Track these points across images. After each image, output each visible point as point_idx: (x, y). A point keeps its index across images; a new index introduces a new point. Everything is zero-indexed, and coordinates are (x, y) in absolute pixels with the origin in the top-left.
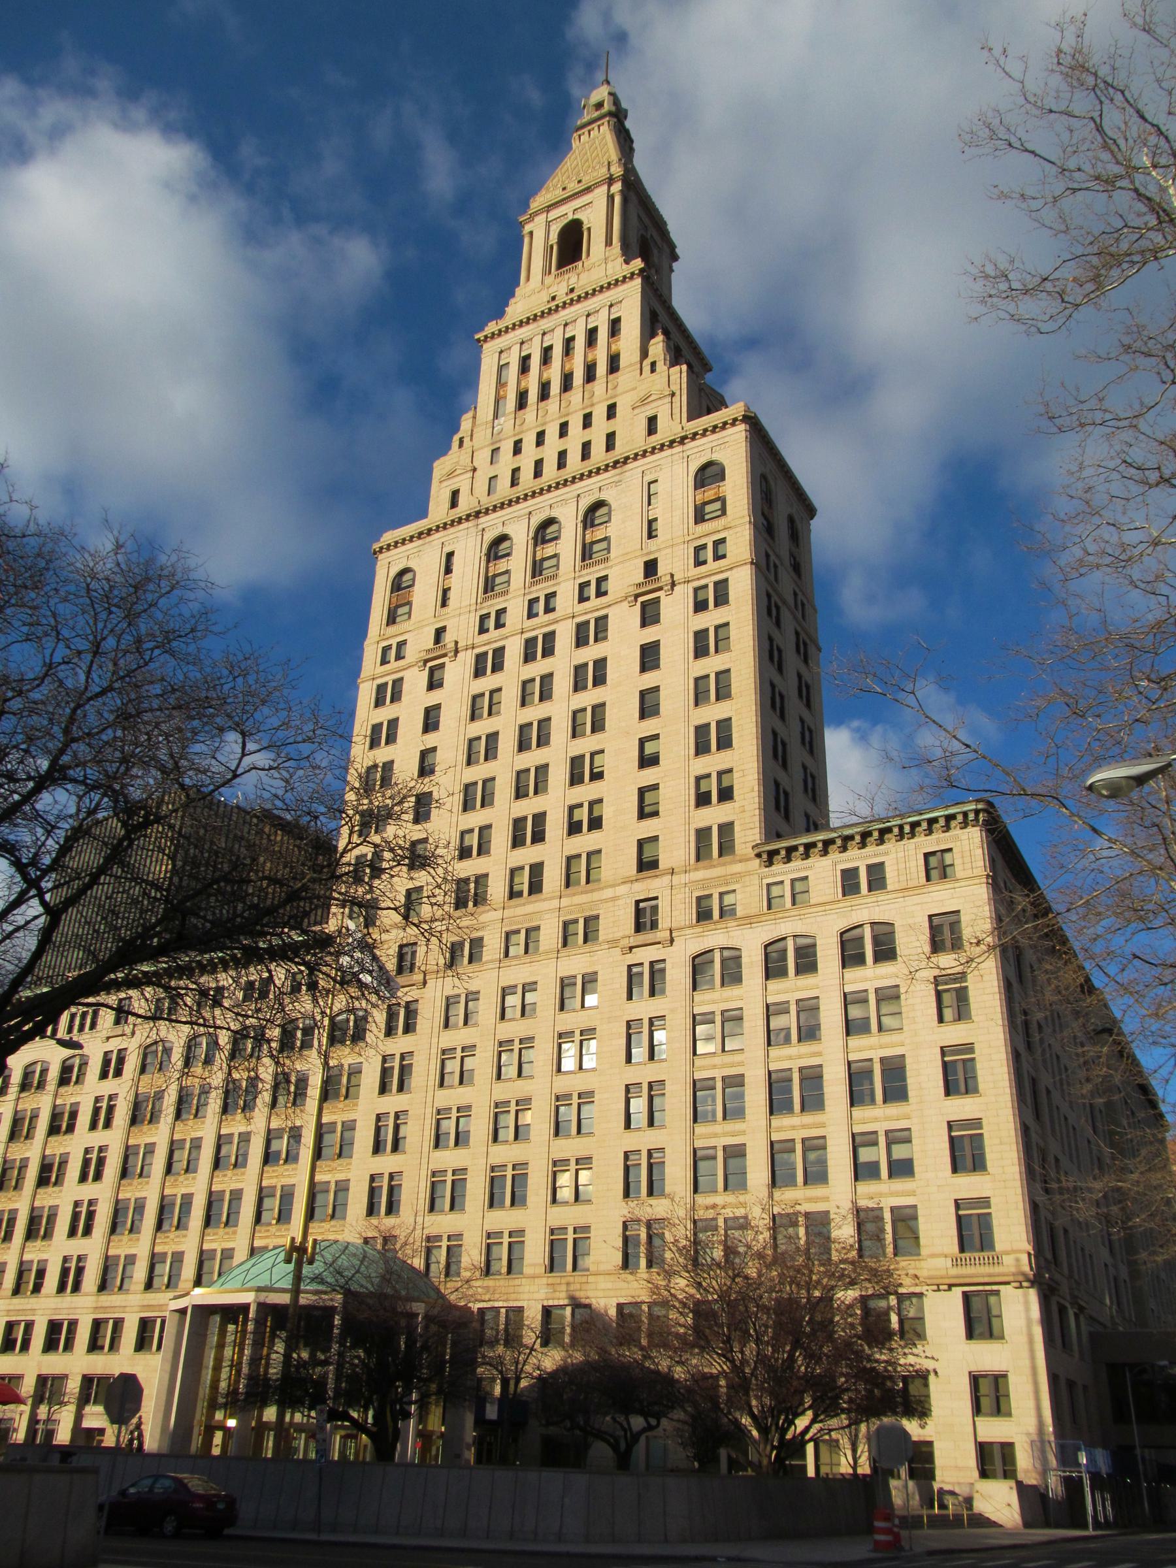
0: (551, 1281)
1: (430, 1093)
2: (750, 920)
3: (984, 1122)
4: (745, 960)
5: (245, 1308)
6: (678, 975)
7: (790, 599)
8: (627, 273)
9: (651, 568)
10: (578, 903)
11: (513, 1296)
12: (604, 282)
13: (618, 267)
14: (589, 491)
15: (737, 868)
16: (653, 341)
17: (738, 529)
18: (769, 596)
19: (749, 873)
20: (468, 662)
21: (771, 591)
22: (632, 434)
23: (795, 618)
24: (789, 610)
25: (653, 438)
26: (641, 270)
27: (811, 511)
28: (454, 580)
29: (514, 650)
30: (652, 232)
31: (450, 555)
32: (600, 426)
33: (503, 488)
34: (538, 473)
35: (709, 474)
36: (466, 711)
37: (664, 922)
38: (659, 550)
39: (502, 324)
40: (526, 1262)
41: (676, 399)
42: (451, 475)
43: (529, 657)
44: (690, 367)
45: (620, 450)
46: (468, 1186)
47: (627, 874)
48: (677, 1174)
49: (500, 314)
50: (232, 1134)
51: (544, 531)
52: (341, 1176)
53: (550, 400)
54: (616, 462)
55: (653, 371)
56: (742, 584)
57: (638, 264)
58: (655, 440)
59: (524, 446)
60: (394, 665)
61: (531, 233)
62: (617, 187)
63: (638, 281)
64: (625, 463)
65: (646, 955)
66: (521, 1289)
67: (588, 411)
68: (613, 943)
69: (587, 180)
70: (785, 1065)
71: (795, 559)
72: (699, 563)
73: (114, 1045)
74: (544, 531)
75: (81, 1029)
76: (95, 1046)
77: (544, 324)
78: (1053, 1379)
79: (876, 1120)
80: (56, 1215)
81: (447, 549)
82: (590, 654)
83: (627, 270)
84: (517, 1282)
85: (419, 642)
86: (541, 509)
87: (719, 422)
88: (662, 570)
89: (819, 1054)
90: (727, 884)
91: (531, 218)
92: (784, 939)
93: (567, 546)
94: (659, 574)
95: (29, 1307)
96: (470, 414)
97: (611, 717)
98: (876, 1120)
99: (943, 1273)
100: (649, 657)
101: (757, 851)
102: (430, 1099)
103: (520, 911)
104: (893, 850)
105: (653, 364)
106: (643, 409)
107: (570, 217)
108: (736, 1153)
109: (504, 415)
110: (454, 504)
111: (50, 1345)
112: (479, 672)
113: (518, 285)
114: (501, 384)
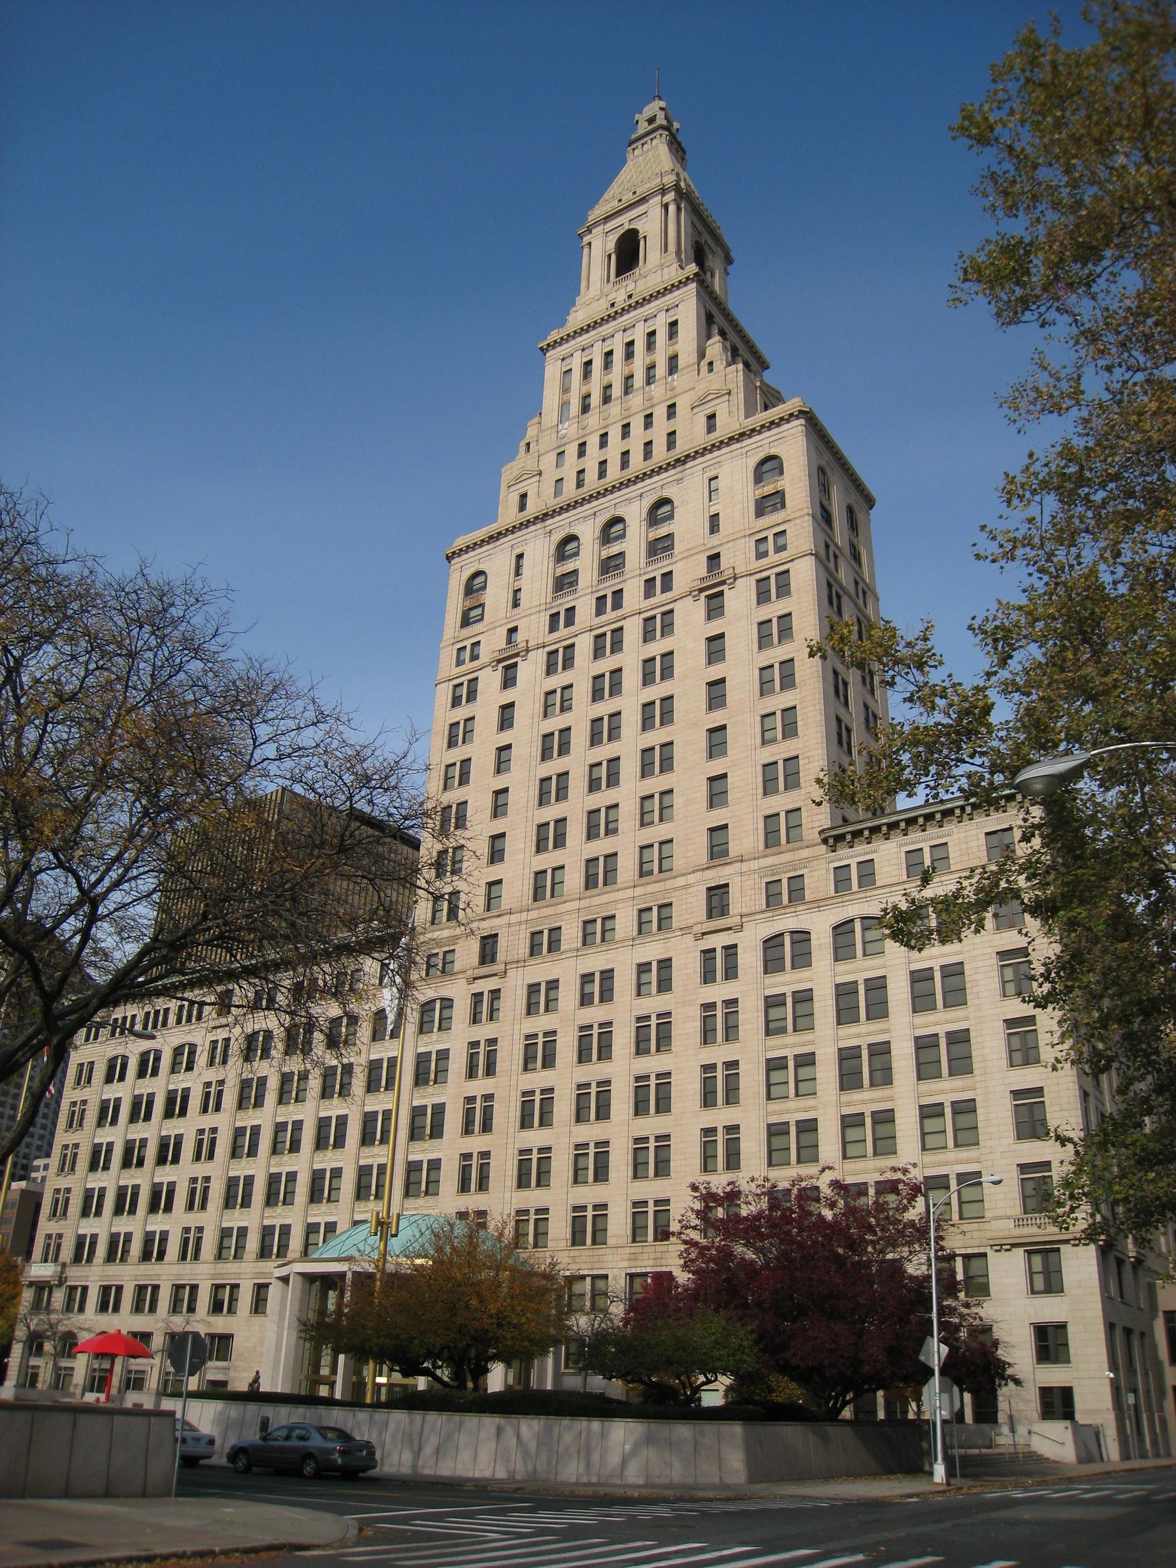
0: (633, 1250)
1: (514, 1078)
2: (819, 904)
3: (1046, 1090)
4: (814, 942)
5: (342, 1275)
6: (750, 958)
7: (851, 588)
8: (682, 278)
9: (714, 559)
10: (653, 892)
11: (597, 1265)
12: (660, 287)
13: (674, 273)
14: (652, 490)
15: (805, 853)
16: (709, 342)
17: (798, 521)
18: (829, 586)
19: (815, 858)
20: (540, 660)
21: (832, 581)
22: (692, 434)
23: (856, 605)
24: (850, 597)
25: (713, 436)
26: (696, 275)
27: (870, 502)
28: (525, 582)
29: (584, 646)
30: (706, 237)
31: (520, 556)
32: (661, 426)
33: (570, 491)
34: (602, 474)
35: (769, 465)
36: (539, 707)
37: (735, 908)
38: (721, 544)
39: (563, 332)
40: (609, 1233)
41: (733, 397)
42: (518, 480)
43: (598, 653)
44: (747, 365)
45: (682, 448)
46: (553, 1163)
47: (699, 862)
48: (753, 1146)
49: (562, 323)
50: (330, 1118)
51: (612, 528)
52: (433, 1156)
53: (612, 403)
54: (677, 461)
55: (711, 370)
56: (804, 574)
57: (693, 268)
58: (716, 436)
59: (588, 447)
60: (468, 666)
61: (590, 244)
62: (670, 196)
63: (693, 286)
64: (684, 463)
65: (718, 942)
66: (605, 1258)
67: (648, 412)
68: (686, 930)
69: (642, 190)
70: (854, 1042)
71: (855, 548)
72: (761, 555)
73: (221, 1035)
74: (612, 528)
75: (155, 1026)
76: (167, 1041)
77: (606, 329)
78: (1110, 1327)
79: (942, 1092)
80: (96, 1243)
81: (518, 551)
82: (656, 648)
83: (682, 275)
84: (602, 1252)
85: (493, 643)
86: (606, 508)
87: (776, 418)
88: (724, 562)
89: (887, 1031)
90: (795, 870)
91: (589, 231)
92: (852, 920)
93: (634, 544)
94: (722, 568)
95: (154, 1272)
96: (536, 420)
97: (679, 708)
98: (942, 1092)
99: (1005, 1234)
100: (715, 646)
101: (823, 836)
102: (514, 1083)
103: (596, 901)
104: (955, 831)
105: (711, 364)
106: (702, 408)
107: (626, 227)
108: (808, 1127)
109: (568, 419)
110: (522, 507)
111: (271, 1200)
112: (550, 669)
113: (578, 294)
114: (566, 390)
